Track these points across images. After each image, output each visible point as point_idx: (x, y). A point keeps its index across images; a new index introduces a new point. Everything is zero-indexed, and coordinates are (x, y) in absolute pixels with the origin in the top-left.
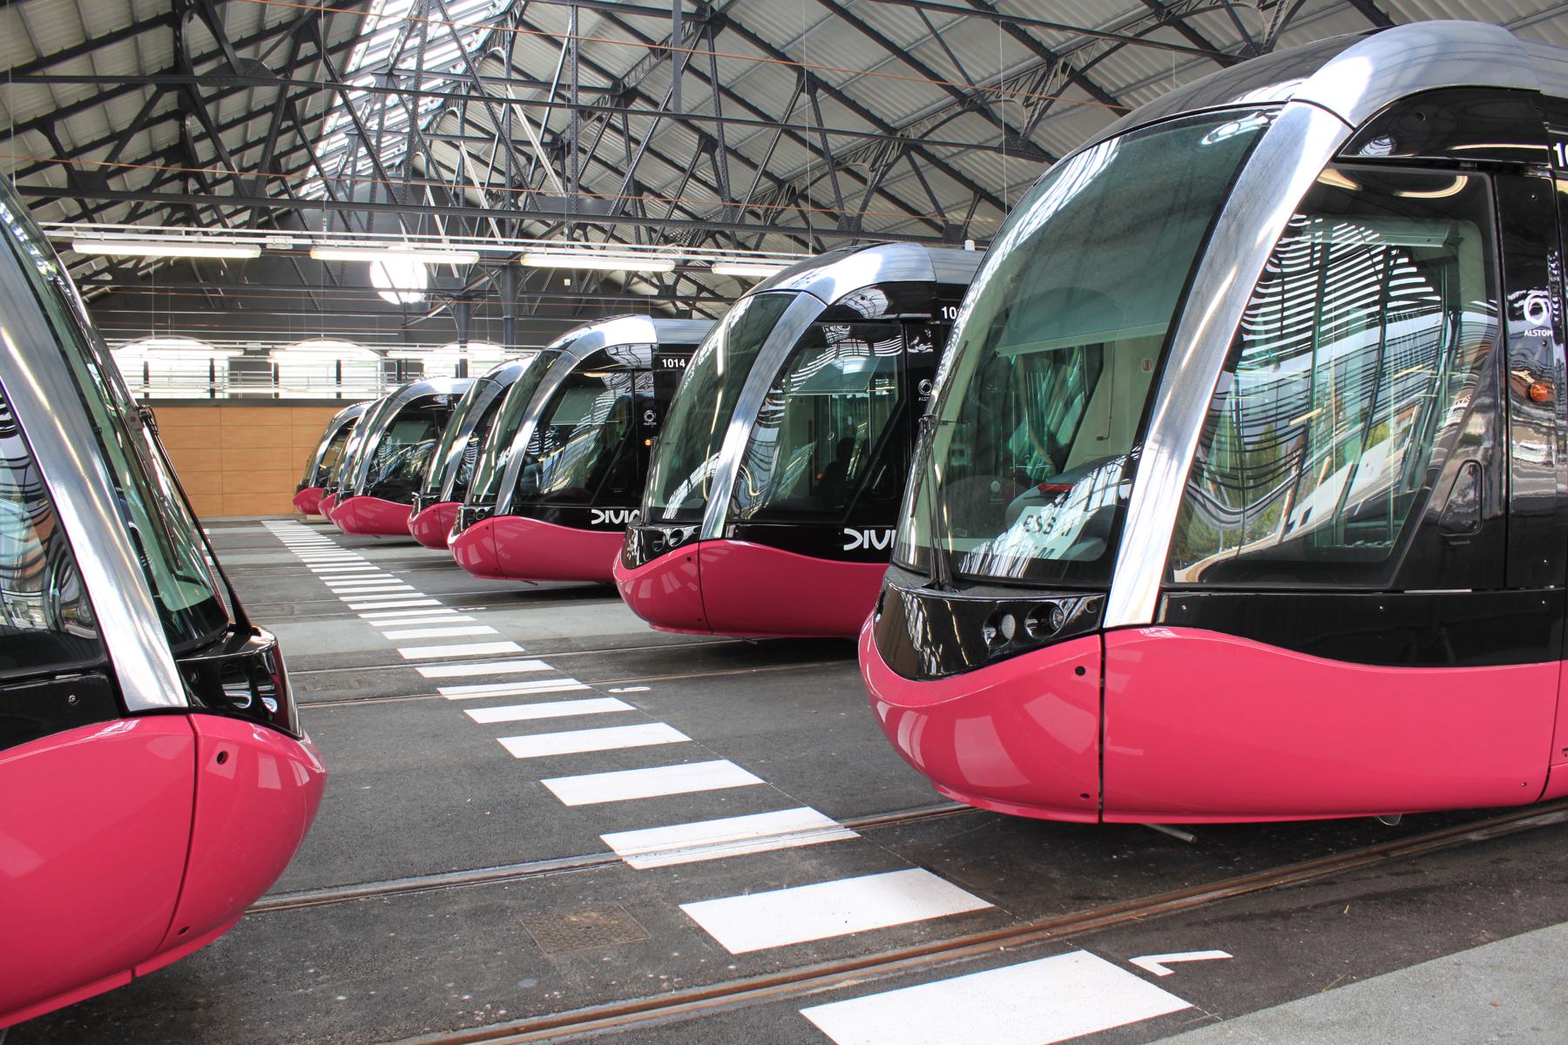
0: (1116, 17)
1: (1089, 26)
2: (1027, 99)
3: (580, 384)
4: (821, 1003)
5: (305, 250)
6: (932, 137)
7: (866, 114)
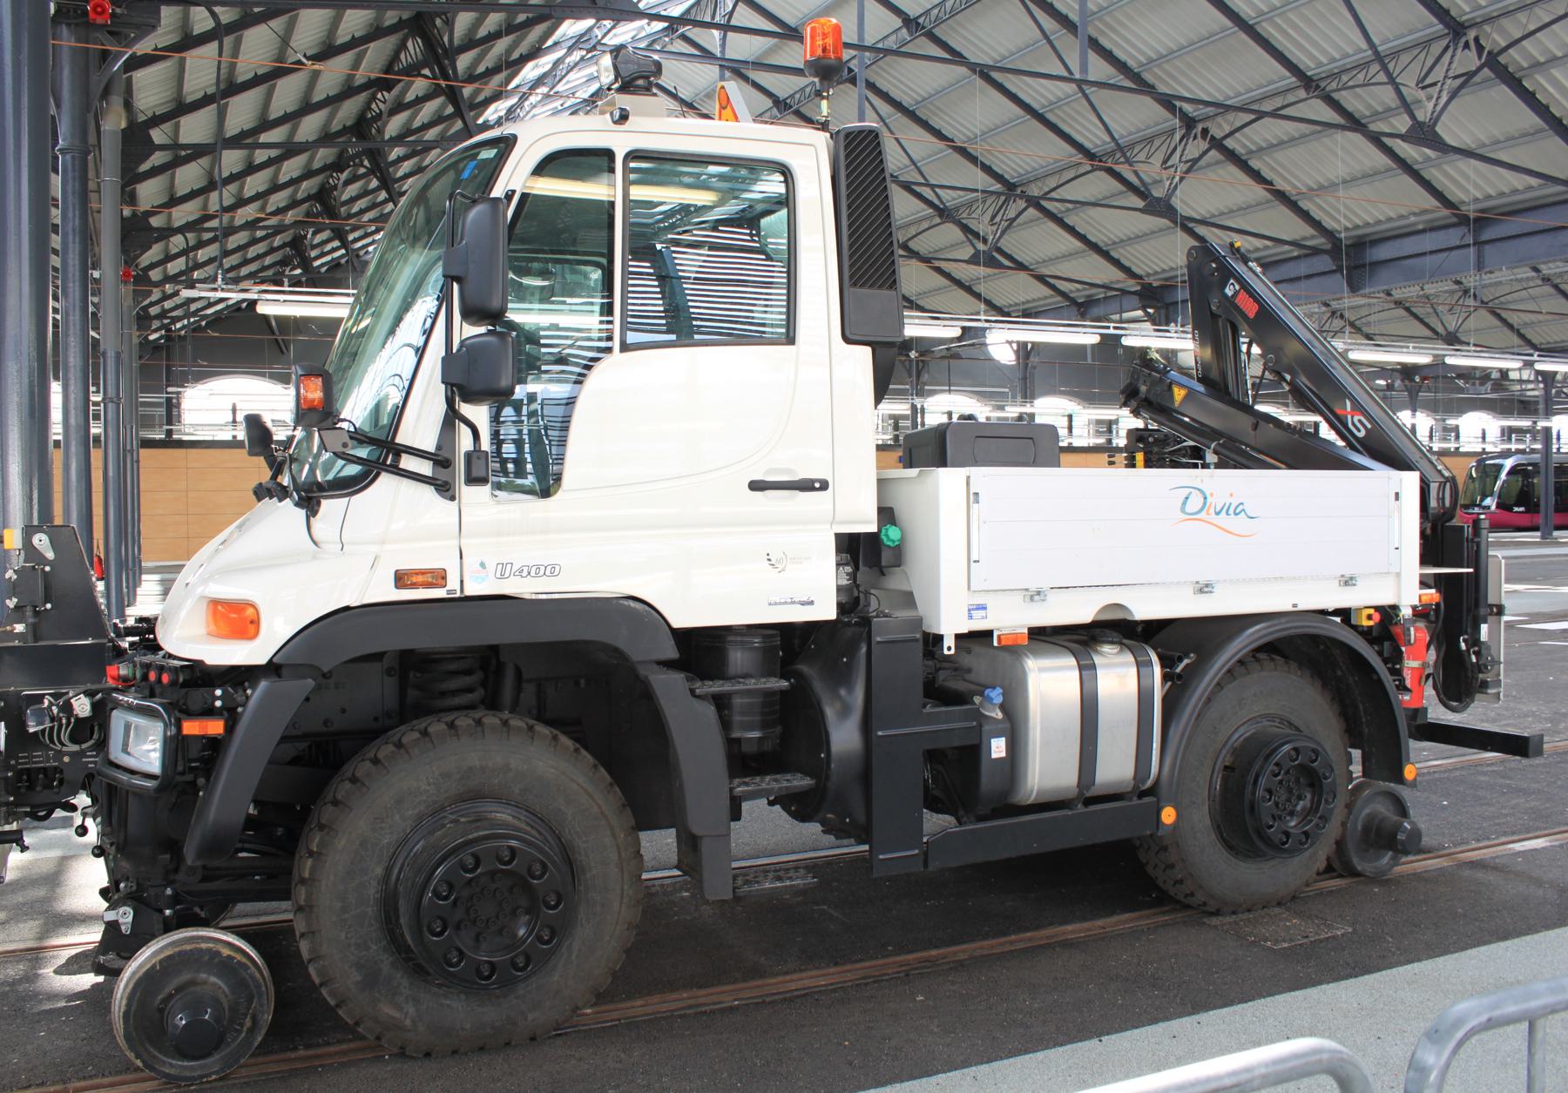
0: (1157, 124)
1: (1220, 98)
2: (1165, 162)
3: (500, 932)
4: (423, 572)
5: (253, 304)
6: (1053, 195)
7: (987, 169)
